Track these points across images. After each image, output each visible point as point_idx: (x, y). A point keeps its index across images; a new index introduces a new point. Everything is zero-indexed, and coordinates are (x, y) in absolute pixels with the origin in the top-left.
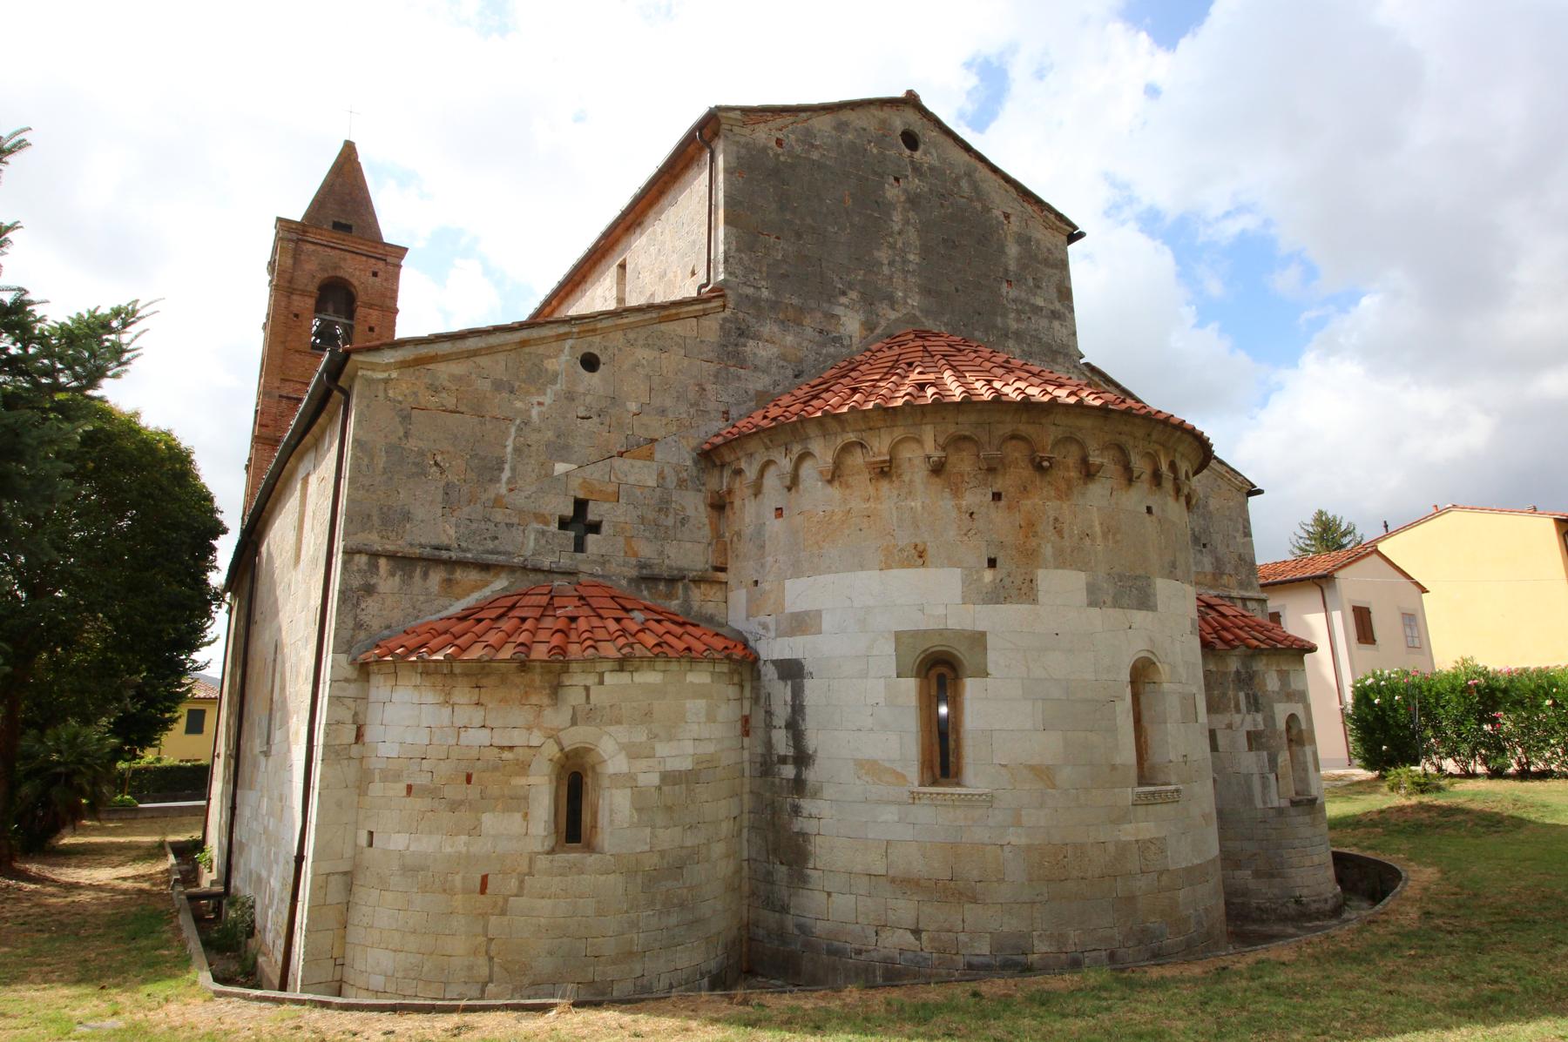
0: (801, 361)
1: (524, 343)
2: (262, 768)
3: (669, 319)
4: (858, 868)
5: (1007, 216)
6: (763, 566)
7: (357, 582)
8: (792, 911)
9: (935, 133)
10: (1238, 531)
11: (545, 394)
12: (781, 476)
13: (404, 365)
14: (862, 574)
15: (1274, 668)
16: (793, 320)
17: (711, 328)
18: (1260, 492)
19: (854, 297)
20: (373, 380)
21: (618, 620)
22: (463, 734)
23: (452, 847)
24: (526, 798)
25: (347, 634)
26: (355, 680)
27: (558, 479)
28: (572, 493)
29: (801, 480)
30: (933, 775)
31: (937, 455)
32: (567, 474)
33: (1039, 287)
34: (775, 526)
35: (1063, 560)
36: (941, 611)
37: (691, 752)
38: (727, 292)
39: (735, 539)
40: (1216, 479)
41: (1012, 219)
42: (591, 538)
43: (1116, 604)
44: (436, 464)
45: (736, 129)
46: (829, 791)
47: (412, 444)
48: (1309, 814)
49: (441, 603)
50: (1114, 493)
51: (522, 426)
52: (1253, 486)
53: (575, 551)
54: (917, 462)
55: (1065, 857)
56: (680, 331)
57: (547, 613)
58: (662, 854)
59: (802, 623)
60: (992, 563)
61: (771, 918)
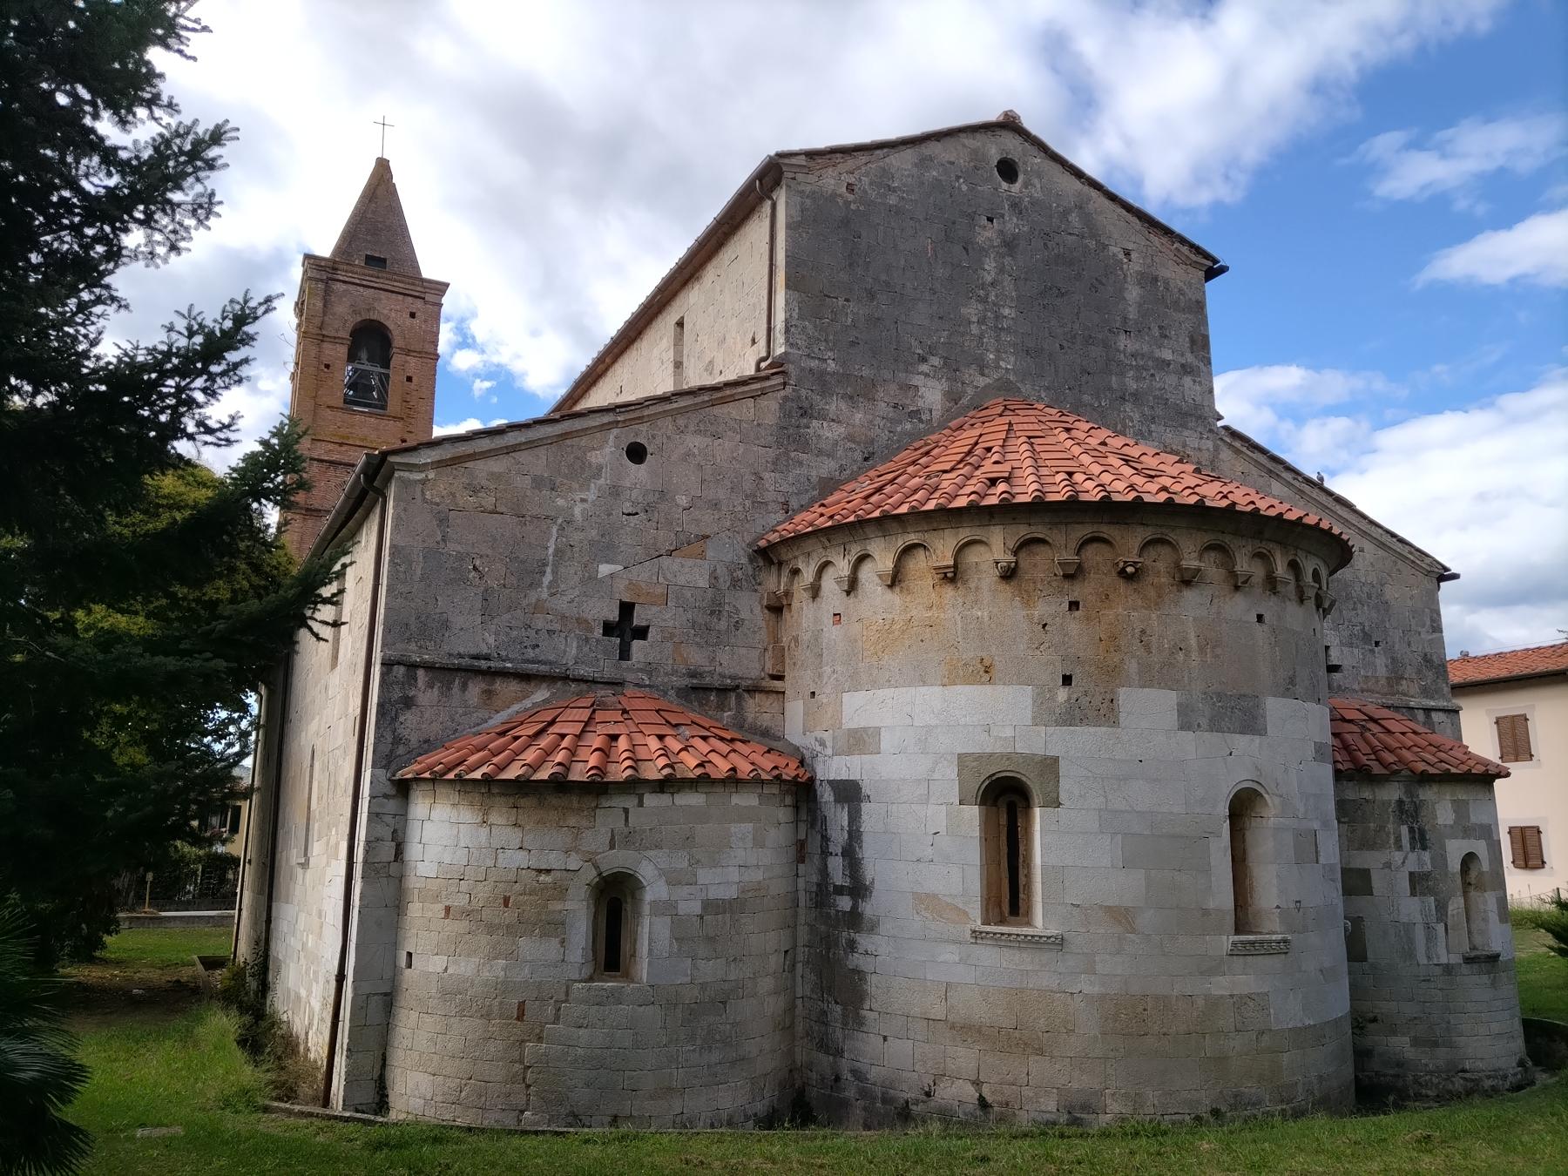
0: (872, 441)
1: (565, 436)
2: (300, 880)
3: (724, 401)
4: (916, 1011)
5: (1127, 254)
6: (820, 676)
7: (397, 694)
8: (846, 1055)
9: (1038, 160)
10: (1424, 626)
11: (588, 490)
12: (839, 581)
13: (439, 464)
14: (923, 690)
15: (1448, 798)
16: (862, 392)
17: (770, 408)
18: (1455, 577)
19: (936, 364)
20: (409, 481)
21: (661, 737)
22: (501, 856)
23: (489, 971)
24: (563, 924)
25: (386, 749)
26: (393, 797)
27: (601, 581)
28: (617, 596)
29: (860, 585)
30: (1001, 913)
31: (1007, 558)
32: (612, 575)
33: (1166, 336)
34: (832, 633)
35: (1149, 679)
36: (1009, 732)
37: (737, 879)
38: (790, 368)
39: (793, 645)
40: (1396, 563)
41: (1134, 256)
42: (637, 645)
43: (1215, 726)
44: (475, 568)
45: (800, 177)
46: (886, 927)
47: (453, 548)
48: (1489, 973)
49: (480, 715)
50: (1215, 601)
51: (564, 525)
52: (1446, 569)
53: (621, 658)
54: (984, 567)
55: (1145, 1010)
56: (734, 414)
57: (588, 729)
58: (703, 986)
59: (861, 741)
60: (1067, 680)
61: (825, 1060)
